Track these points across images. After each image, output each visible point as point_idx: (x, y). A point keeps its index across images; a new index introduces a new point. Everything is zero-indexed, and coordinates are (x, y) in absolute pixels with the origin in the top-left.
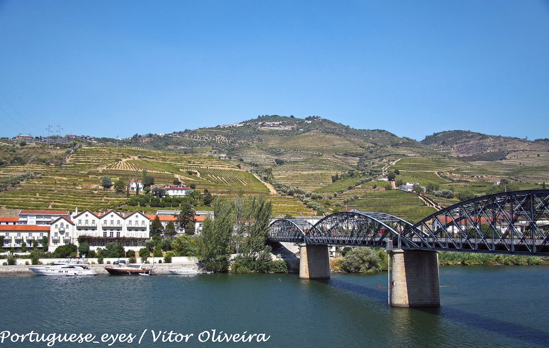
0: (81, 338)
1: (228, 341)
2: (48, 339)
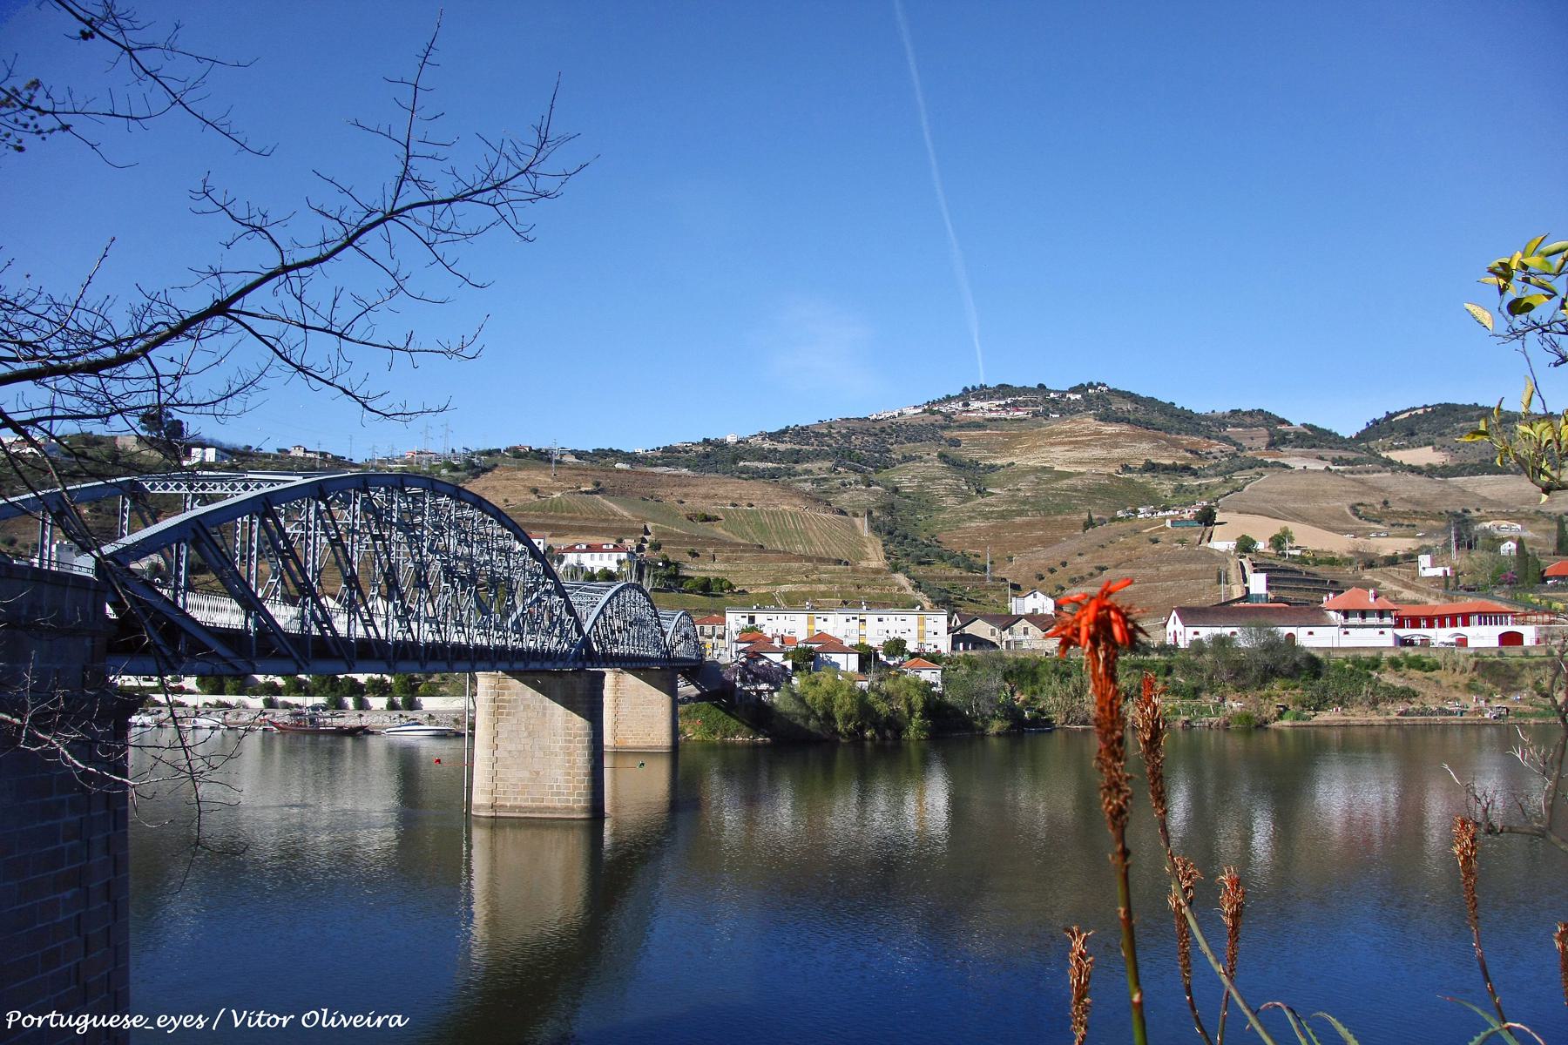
1: (346, 1025)
2: (77, 1023)
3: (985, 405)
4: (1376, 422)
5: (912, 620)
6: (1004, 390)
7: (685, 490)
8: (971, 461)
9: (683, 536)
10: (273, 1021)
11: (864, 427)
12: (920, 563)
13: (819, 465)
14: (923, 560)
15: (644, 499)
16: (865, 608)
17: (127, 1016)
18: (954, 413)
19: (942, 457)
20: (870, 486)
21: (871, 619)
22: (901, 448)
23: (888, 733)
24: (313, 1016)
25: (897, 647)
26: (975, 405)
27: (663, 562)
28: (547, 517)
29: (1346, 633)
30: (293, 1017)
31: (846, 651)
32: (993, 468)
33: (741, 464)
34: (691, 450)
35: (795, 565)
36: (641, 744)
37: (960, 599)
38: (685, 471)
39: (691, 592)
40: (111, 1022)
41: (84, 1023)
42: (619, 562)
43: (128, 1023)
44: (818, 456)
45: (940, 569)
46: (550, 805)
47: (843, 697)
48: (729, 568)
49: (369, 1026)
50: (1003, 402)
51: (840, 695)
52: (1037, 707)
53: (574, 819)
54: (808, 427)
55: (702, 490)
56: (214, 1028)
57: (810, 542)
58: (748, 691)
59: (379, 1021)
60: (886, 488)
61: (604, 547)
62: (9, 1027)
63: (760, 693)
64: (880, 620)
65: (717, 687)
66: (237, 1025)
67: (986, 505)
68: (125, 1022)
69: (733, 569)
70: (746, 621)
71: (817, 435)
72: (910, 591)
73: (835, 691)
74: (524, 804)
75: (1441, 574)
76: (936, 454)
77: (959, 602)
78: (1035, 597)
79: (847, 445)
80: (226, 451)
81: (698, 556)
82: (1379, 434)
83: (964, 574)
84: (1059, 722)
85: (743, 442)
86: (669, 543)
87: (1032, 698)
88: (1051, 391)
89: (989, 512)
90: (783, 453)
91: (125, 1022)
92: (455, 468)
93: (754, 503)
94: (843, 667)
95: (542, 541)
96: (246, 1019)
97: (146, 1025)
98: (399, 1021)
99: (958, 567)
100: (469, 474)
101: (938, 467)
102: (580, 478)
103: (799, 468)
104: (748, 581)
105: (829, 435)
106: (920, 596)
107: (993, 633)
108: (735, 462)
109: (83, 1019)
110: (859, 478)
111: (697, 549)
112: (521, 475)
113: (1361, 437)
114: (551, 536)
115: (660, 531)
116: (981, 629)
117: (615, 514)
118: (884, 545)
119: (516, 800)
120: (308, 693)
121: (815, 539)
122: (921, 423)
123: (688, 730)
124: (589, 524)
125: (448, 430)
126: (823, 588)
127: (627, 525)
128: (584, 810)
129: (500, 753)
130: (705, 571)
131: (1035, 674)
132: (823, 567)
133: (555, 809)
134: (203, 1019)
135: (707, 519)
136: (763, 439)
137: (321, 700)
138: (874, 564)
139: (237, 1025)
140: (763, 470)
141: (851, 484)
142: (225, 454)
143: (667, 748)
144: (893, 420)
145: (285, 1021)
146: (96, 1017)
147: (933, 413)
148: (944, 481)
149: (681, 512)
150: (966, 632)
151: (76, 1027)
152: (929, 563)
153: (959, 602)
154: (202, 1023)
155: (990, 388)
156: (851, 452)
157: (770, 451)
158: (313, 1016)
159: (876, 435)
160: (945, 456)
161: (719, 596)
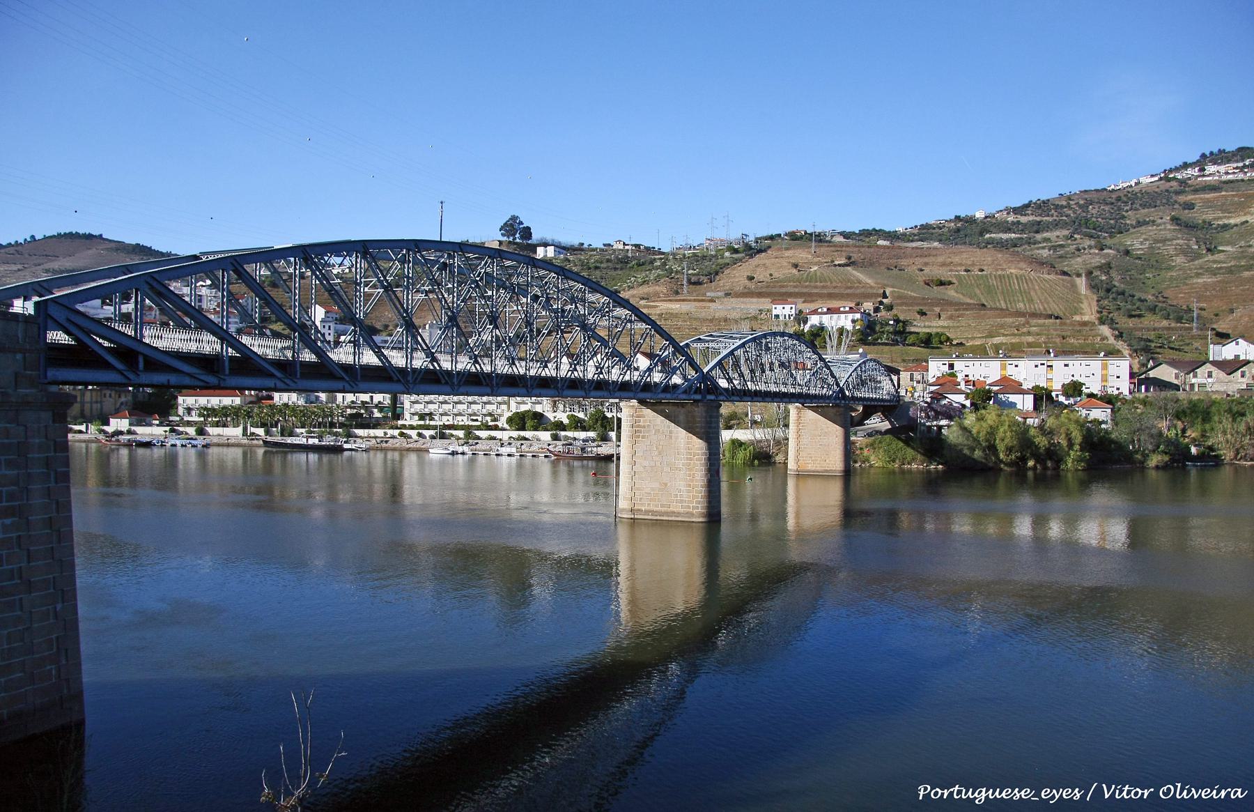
0: (1017, 793)
1: (1196, 797)
2: (976, 795)
3: (1222, 169)
5: (1095, 365)
7: (926, 260)
8: (1204, 222)
9: (915, 298)
10: (1136, 794)
11: (1091, 198)
12: (1131, 316)
13: (1058, 233)
14: (1133, 313)
15: (889, 269)
16: (1052, 355)
17: (1017, 789)
18: (1190, 179)
19: (1175, 220)
20: (1102, 249)
21: (1058, 364)
22: (1136, 214)
23: (1049, 464)
24: (1169, 789)
25: (1074, 389)
26: (1211, 169)
27: (894, 320)
28: (802, 287)
30: (1152, 790)
31: (1023, 392)
32: (1225, 227)
33: (987, 236)
34: (944, 226)
35: (1009, 320)
36: (818, 469)
37: (1160, 347)
38: (936, 244)
39: (913, 345)
40: (1004, 794)
41: (981, 795)
42: (854, 321)
43: (1018, 795)
44: (1056, 225)
45: (1150, 321)
46: (675, 510)
47: (1005, 432)
48: (951, 325)
49: (1215, 797)
50: (1241, 164)
51: (1002, 430)
52: (1206, 443)
53: (693, 522)
54: (1048, 200)
55: (940, 259)
56: (1088, 799)
57: (1031, 301)
58: (930, 427)
59: (1223, 793)
60: (1118, 251)
61: (842, 309)
62: (921, 798)
63: (940, 428)
64: (1066, 365)
65: (905, 423)
66: (1107, 796)
67: (1215, 262)
68: (1015, 794)
69: (955, 324)
70: (946, 368)
71: (1057, 207)
72: (1112, 340)
73: (998, 427)
74: (655, 509)
76: (1169, 218)
77: (1158, 350)
78: (1237, 344)
79: (1084, 214)
80: (564, 248)
81: (926, 314)
83: (1173, 325)
84: (1228, 458)
85: (990, 217)
86: (901, 304)
87: (1203, 436)
89: (1216, 268)
90: (1025, 225)
91: (1015, 794)
92: (736, 251)
93: (985, 268)
94: (1019, 406)
95: (793, 306)
96: (1114, 791)
97: (1032, 797)
98: (1239, 793)
99: (1167, 318)
100: (746, 255)
101: (1169, 230)
102: (836, 253)
103: (1039, 237)
104: (966, 335)
105: (1069, 206)
106: (1120, 345)
107: (1177, 377)
108: (981, 234)
109: (981, 791)
110: (1093, 243)
111: (925, 309)
112: (788, 253)
114: (804, 302)
115: (896, 295)
116: (1165, 373)
117: (860, 282)
118: (1098, 301)
119: (650, 505)
120: (584, 429)
121: (1035, 298)
122: (1157, 190)
123: (872, 458)
124: (836, 291)
125: (728, 220)
126: (1030, 339)
127: (870, 291)
128: (703, 515)
129: (637, 468)
130: (929, 327)
131: (1208, 413)
132: (1034, 321)
133: (679, 514)
134: (1079, 792)
135: (941, 283)
136: (1008, 214)
137: (592, 434)
138: (1086, 318)
139: (1107, 796)
140: (1007, 240)
141: (1084, 249)
142: (561, 251)
143: (840, 472)
144: (1130, 190)
145: (1146, 793)
146: (991, 790)
147: (1169, 180)
148: (1175, 242)
149: (920, 279)
150: (1151, 376)
151: (975, 798)
152: (1140, 316)
153: (1158, 350)
154: (1078, 795)
155: (1229, 152)
156: (1087, 220)
157: (1013, 223)
158: (1169, 789)
159: (1112, 203)
160: (1177, 219)
161: (938, 348)
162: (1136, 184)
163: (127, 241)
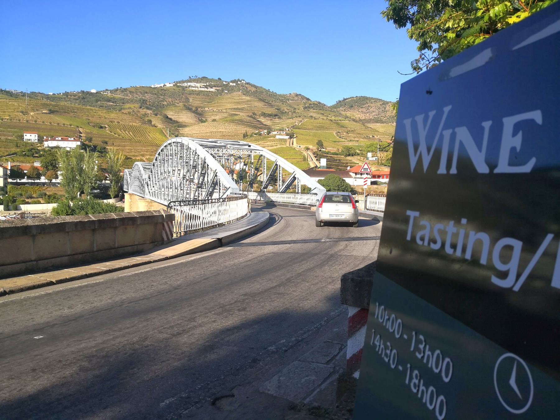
3: (198, 85)
4: (340, 102)
6: (204, 79)
29: (356, 180)
44: (132, 101)
50: (205, 84)
71: (131, 92)
75: (375, 160)
82: (341, 105)
88: (223, 81)
113: (334, 107)
147: (178, 87)
162: (164, 86)
163: (264, 87)
